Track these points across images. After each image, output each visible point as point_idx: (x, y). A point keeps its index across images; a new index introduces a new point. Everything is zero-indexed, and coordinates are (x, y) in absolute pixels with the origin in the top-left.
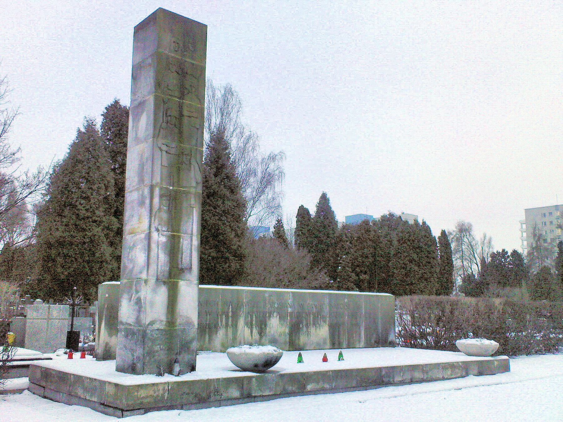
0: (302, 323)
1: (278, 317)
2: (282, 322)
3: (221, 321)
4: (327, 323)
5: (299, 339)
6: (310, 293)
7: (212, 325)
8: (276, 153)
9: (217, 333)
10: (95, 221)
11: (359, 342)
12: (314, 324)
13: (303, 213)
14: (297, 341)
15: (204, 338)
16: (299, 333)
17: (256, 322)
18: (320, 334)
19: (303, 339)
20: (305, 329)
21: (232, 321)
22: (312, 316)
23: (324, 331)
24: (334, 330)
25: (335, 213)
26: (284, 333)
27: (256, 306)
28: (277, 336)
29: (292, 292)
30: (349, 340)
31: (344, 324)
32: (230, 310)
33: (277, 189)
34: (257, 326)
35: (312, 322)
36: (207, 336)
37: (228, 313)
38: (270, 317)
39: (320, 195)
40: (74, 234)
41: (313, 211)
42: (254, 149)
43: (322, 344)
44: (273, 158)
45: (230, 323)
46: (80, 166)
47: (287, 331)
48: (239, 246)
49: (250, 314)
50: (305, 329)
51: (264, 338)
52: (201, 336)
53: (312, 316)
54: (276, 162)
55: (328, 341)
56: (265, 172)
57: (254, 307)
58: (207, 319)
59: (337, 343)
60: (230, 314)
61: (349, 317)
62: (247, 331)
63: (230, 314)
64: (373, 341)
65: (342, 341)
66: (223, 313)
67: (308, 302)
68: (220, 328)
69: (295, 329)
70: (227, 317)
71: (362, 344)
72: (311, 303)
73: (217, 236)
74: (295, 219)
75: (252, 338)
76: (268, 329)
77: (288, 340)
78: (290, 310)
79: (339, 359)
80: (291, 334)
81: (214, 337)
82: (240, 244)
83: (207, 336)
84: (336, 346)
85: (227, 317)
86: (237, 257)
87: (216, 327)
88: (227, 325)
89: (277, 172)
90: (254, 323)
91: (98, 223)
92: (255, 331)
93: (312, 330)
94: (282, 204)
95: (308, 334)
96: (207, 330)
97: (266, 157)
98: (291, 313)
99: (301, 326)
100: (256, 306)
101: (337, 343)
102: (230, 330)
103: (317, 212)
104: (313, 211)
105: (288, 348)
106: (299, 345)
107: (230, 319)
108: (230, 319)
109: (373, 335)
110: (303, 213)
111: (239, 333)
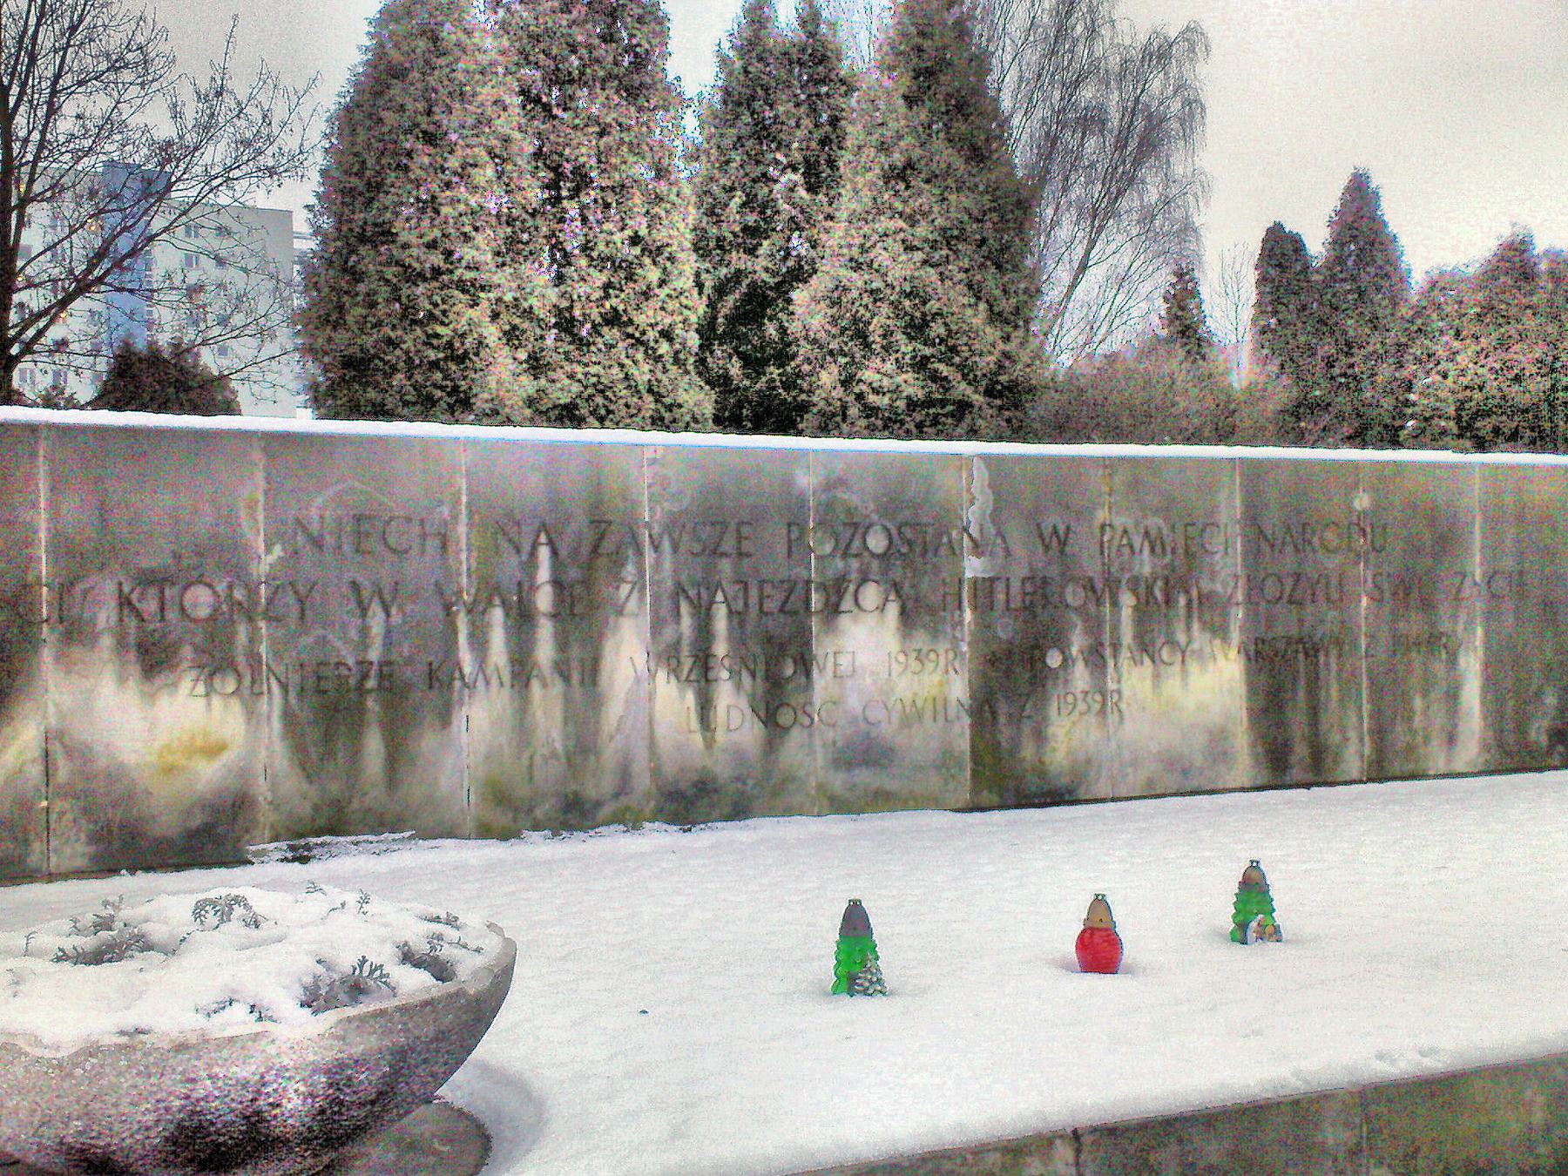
0: (1062, 644)
1: (893, 609)
2: (921, 639)
3: (480, 643)
4: (1236, 637)
5: (1040, 737)
6: (1109, 464)
7: (413, 675)
8: (1173, 35)
9: (445, 718)
10: (462, 286)
11: (1451, 740)
12: (1145, 646)
13: (1280, 250)
14: (1028, 752)
15: (356, 753)
16: (1044, 700)
17: (738, 640)
18: (1190, 702)
19: (1068, 734)
20: (1080, 677)
21: (562, 644)
22: (1127, 600)
23: (1210, 684)
24: (1284, 676)
25: (1403, 240)
26: (939, 705)
27: (729, 544)
28: (888, 730)
29: (987, 459)
30: (1380, 733)
31: (1342, 641)
32: (544, 574)
33: (1179, 170)
34: (742, 661)
35: (1127, 637)
36: (374, 745)
37: (526, 589)
38: (833, 610)
39: (1341, 181)
40: (392, 334)
41: (1317, 243)
42: (1092, 32)
43: (1199, 760)
44: (1159, 54)
45: (545, 650)
46: (396, 89)
47: (959, 689)
48: (1006, 355)
49: (695, 596)
50: (1080, 677)
51: (796, 735)
52: (328, 737)
53: (1127, 600)
54: (1173, 70)
55: (1242, 741)
56: (1132, 110)
57: (716, 553)
58: (364, 632)
59: (1301, 751)
60: (544, 600)
61: (1377, 600)
62: (672, 701)
63: (544, 600)
64: (1538, 733)
65: (1335, 738)
66: (490, 590)
67: (1102, 515)
68: (470, 687)
69: (1014, 675)
70: (522, 617)
71: (1470, 750)
72: (1120, 521)
73: (925, 324)
74: (1251, 276)
75: (709, 743)
76: (822, 683)
77: (963, 744)
78: (973, 567)
79: (1241, 934)
80: (983, 709)
81: (427, 741)
82: (1009, 347)
83: (374, 745)
84: (1296, 773)
85: (522, 617)
86: (1000, 395)
87: (441, 680)
88: (522, 669)
89: (1176, 106)
90: (721, 648)
91: (473, 290)
92: (731, 700)
93: (1132, 678)
94: (1197, 220)
95: (1105, 702)
96: (372, 704)
97: (1135, 54)
98: (984, 591)
99: (1054, 660)
100: (729, 544)
101: (1301, 751)
102: (547, 703)
103: (1337, 242)
104: (1317, 243)
105: (965, 796)
106: (1042, 773)
107: (545, 632)
108: (545, 632)
109: (1538, 694)
110: (1280, 250)
111: (614, 710)
